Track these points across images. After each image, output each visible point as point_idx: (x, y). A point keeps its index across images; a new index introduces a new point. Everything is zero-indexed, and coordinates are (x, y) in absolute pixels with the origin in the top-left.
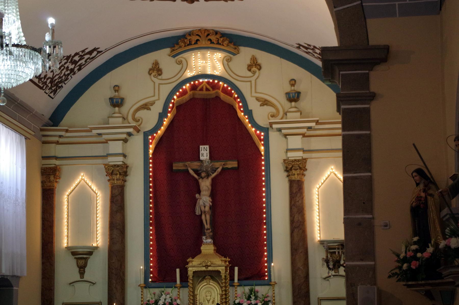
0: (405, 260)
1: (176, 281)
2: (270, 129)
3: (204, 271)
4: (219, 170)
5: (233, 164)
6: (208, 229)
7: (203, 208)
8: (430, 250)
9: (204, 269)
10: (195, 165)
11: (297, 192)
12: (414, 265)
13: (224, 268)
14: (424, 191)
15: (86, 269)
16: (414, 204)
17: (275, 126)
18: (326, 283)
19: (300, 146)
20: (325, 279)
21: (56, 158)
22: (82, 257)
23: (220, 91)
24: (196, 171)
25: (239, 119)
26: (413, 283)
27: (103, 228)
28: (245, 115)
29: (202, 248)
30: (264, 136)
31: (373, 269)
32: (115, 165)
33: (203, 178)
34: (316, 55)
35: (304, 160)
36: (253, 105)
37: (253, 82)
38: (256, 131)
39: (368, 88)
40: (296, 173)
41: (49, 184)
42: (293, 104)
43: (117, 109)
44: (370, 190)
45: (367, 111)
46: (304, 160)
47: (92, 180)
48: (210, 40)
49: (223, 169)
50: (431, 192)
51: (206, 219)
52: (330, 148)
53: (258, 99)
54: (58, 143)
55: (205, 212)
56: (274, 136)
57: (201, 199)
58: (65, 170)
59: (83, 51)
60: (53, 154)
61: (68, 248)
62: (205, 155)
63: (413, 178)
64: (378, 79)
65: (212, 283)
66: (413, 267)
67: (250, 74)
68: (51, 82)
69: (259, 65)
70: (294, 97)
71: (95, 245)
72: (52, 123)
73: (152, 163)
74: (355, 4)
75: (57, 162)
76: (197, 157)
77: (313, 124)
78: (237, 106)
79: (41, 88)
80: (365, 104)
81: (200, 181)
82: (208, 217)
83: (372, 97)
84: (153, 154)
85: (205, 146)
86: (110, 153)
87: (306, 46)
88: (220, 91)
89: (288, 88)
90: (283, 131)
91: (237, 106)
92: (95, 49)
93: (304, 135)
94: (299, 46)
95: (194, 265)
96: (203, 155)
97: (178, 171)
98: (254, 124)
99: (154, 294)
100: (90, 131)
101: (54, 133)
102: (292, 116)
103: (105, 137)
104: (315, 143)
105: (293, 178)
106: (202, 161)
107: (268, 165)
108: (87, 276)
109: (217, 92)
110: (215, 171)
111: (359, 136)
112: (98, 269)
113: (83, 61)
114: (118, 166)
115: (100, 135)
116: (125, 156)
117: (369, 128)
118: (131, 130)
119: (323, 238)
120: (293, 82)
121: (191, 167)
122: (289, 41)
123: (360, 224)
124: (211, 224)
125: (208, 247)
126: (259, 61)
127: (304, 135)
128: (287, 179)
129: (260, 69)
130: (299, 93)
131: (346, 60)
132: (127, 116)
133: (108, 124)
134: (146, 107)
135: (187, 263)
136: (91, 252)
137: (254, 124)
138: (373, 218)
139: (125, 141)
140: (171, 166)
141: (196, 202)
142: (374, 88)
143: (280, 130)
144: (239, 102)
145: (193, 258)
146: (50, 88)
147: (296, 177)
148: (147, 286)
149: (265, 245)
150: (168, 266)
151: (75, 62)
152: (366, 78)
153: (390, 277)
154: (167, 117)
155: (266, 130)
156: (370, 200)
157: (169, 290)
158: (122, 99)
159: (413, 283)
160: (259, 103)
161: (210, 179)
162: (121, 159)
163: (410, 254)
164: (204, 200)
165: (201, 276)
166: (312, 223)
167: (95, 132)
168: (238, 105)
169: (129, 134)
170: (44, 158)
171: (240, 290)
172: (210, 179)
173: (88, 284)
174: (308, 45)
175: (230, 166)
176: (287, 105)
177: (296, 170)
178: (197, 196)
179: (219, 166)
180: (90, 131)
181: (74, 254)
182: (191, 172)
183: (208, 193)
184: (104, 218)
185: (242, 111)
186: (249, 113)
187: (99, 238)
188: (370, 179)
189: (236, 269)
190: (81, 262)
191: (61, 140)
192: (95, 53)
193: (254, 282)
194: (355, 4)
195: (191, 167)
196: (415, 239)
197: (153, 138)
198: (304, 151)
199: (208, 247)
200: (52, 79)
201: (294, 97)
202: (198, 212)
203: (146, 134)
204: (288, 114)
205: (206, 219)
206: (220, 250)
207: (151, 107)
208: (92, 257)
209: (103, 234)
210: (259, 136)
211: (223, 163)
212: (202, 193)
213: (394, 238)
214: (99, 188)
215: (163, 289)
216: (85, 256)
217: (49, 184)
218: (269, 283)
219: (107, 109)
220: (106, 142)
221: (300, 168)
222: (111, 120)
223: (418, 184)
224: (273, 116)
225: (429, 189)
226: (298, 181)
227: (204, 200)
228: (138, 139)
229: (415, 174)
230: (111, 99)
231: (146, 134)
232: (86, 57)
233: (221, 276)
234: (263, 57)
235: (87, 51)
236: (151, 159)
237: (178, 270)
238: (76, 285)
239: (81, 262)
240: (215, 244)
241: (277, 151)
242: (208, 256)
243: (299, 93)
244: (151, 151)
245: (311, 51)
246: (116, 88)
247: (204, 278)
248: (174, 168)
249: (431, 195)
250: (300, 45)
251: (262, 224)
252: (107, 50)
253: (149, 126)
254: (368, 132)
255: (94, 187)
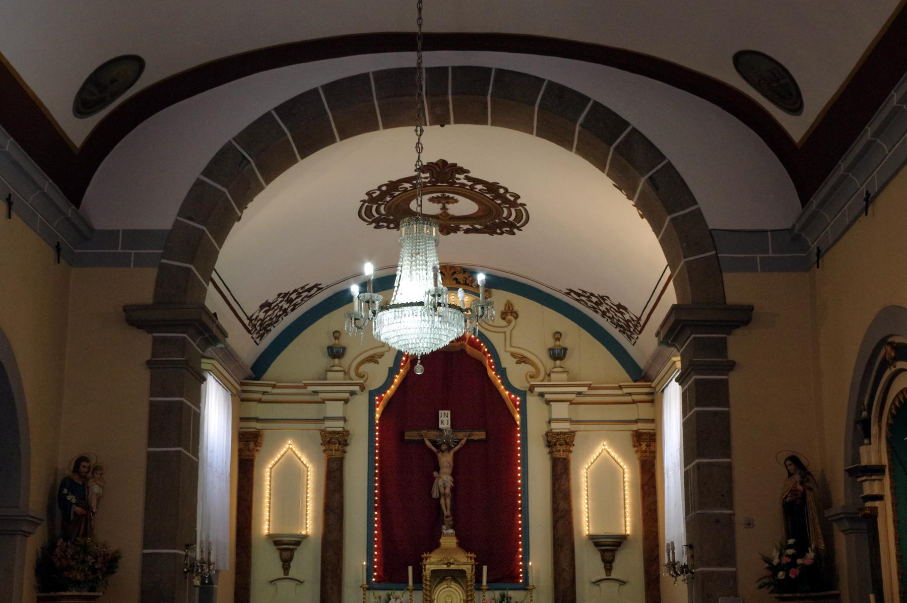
0: (780, 567)
1: (407, 582)
2: (528, 393)
3: (445, 570)
4: (463, 442)
5: (480, 435)
6: (447, 517)
7: (442, 490)
8: (811, 555)
9: (445, 567)
10: (433, 434)
11: (561, 473)
12: (794, 573)
13: (470, 567)
14: (802, 483)
15: (292, 564)
16: (788, 499)
17: (537, 390)
18: (596, 589)
19: (566, 416)
20: (594, 583)
21: (257, 420)
22: (287, 547)
23: (466, 343)
24: (434, 443)
25: (489, 379)
26: (790, 595)
27: (316, 511)
28: (496, 374)
29: (441, 541)
30: (520, 401)
31: (734, 576)
32: (334, 432)
33: (442, 452)
34: (589, 303)
35: (572, 434)
36: (507, 361)
37: (508, 333)
38: (510, 395)
39: (726, 357)
40: (561, 449)
41: (248, 453)
42: (558, 362)
43: (337, 360)
44: (730, 479)
45: (725, 383)
46: (572, 434)
47: (302, 449)
48: (456, 279)
49: (467, 441)
50: (808, 484)
51: (446, 504)
52: (602, 419)
53: (513, 355)
54: (260, 401)
55: (445, 494)
56: (533, 402)
57: (440, 478)
58: (267, 436)
59: (302, 288)
60: (253, 415)
61: (269, 536)
62: (445, 422)
63: (786, 467)
64: (738, 345)
65: (454, 585)
66: (792, 576)
67: (504, 323)
68: (261, 325)
69: (516, 313)
70: (558, 354)
71: (303, 533)
72: (254, 376)
73: (380, 431)
74: (709, 254)
75: (259, 426)
76: (436, 427)
77: (584, 389)
78: (487, 362)
79: (249, 332)
80: (723, 375)
81: (440, 455)
82: (448, 501)
83: (731, 366)
84: (380, 419)
85: (446, 412)
86: (328, 415)
87: (580, 292)
88: (466, 343)
89: (551, 343)
90: (547, 396)
91: (487, 362)
92: (316, 286)
93: (571, 402)
94: (570, 292)
95: (433, 563)
96: (442, 422)
97: (410, 442)
98: (509, 386)
99: (380, 598)
100: (305, 386)
101: (256, 389)
102: (557, 378)
103: (322, 395)
104: (584, 412)
105: (558, 455)
106: (441, 430)
107: (525, 438)
108: (293, 573)
109: (462, 345)
110: (458, 443)
111: (716, 413)
112: (307, 563)
113: (299, 300)
114: (338, 433)
115: (316, 392)
116: (344, 419)
117: (727, 404)
118: (356, 388)
119: (592, 532)
120: (558, 336)
121: (428, 437)
122: (556, 285)
123: (717, 521)
124: (451, 510)
125: (449, 540)
126: (516, 308)
127: (571, 402)
128: (548, 456)
129: (516, 318)
130: (565, 349)
131: (698, 321)
132: (349, 369)
133: (326, 379)
134: (373, 359)
135: (422, 560)
136: (299, 541)
137: (509, 386)
138: (734, 515)
139: (346, 401)
140: (402, 435)
141: (432, 482)
142: (732, 355)
143: (542, 395)
144: (489, 358)
145: (431, 552)
146: (258, 333)
147: (561, 455)
148: (370, 587)
149: (520, 539)
150: (397, 560)
151: (290, 301)
152: (724, 342)
153: (760, 587)
154: (398, 373)
155: (523, 394)
156: (730, 491)
157: (399, 593)
158: (344, 349)
159: (790, 595)
160: (516, 360)
161: (452, 453)
162: (341, 424)
163: (785, 560)
164: (444, 480)
165: (440, 576)
166: (579, 512)
167: (310, 389)
168: (488, 361)
169: (353, 393)
170: (243, 419)
171: (489, 595)
172: (452, 453)
173: (293, 583)
174: (583, 291)
175: (476, 438)
176: (550, 363)
177: (560, 445)
178: (435, 473)
179: (463, 436)
180: (305, 386)
181: (276, 543)
182: (428, 443)
183: (449, 471)
184: (316, 498)
185: (493, 370)
186: (502, 372)
187: (309, 524)
188: (729, 466)
189: (485, 568)
190: (286, 555)
191: (265, 398)
192: (315, 289)
193: (508, 585)
194: (709, 254)
195: (428, 437)
196: (791, 541)
197: (381, 399)
198: (572, 422)
199: (449, 540)
200: (262, 320)
201: (558, 354)
202: (435, 495)
203: (372, 394)
204: (552, 375)
205: (446, 504)
206: (464, 544)
207: (379, 360)
208: (299, 548)
209: (315, 519)
210: (514, 401)
211: (468, 434)
212: (441, 471)
213: (759, 539)
214: (311, 459)
215: (390, 592)
216: (291, 547)
217: (248, 453)
218: (525, 587)
219: (323, 361)
220: (323, 401)
221: (567, 443)
222: (330, 374)
223: (790, 475)
224: (532, 377)
225: (808, 481)
226: (565, 459)
227: (444, 480)
228: (362, 400)
229: (788, 462)
230: (330, 348)
231: (372, 394)
232: (304, 294)
233: (466, 577)
234: (520, 303)
235: (307, 287)
236: (377, 425)
237: (410, 568)
238: (279, 583)
239: (286, 555)
240: (457, 535)
241: (536, 421)
242: (449, 551)
243: (565, 349)
244: (378, 416)
245: (585, 299)
246: (337, 335)
247: (443, 580)
248: (406, 438)
249: (810, 489)
250: (571, 291)
251: (514, 512)
252: (328, 287)
253: (376, 382)
254: (726, 409)
255: (304, 459)
